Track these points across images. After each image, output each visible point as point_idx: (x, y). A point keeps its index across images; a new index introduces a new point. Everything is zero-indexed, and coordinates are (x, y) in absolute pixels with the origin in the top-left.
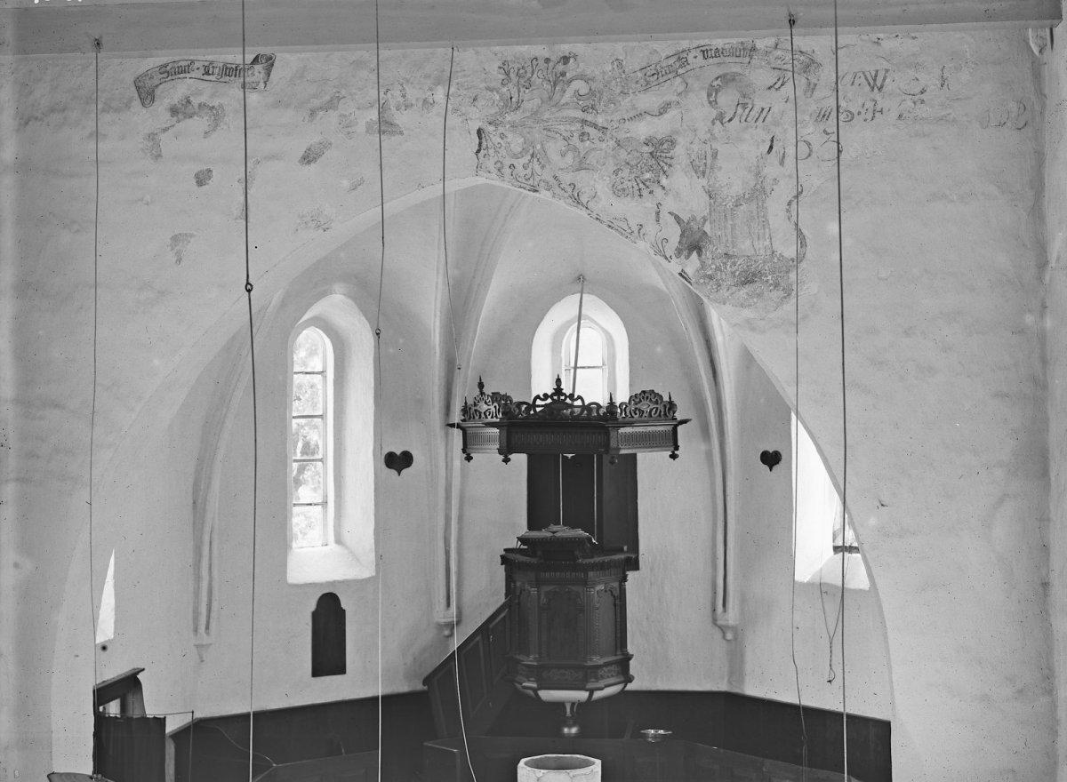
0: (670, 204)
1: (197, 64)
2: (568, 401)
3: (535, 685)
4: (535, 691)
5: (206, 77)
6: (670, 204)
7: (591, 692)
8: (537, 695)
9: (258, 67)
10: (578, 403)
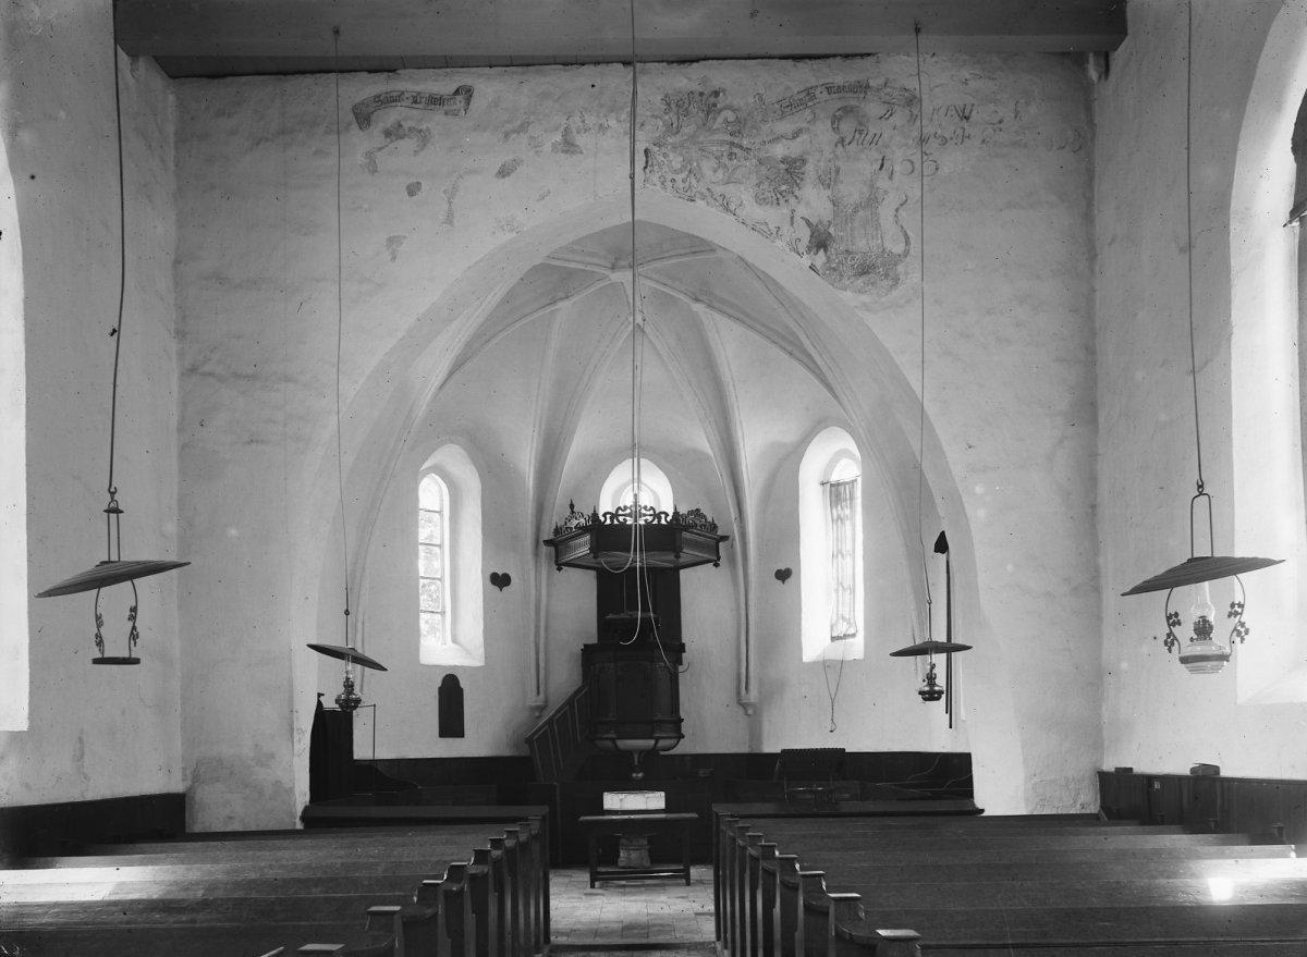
0: (802, 211)
1: (406, 95)
2: (643, 511)
3: (614, 736)
4: (613, 740)
5: (414, 105)
6: (802, 211)
7: (657, 740)
8: (616, 745)
9: (459, 98)
10: (651, 512)
